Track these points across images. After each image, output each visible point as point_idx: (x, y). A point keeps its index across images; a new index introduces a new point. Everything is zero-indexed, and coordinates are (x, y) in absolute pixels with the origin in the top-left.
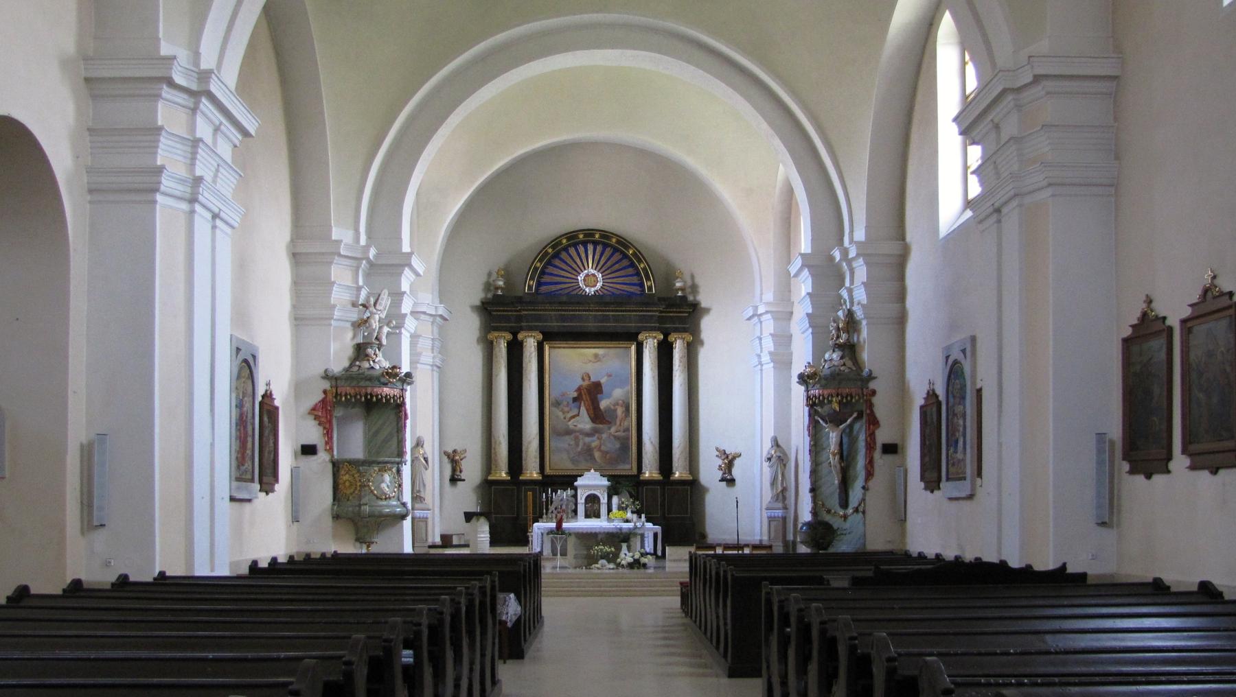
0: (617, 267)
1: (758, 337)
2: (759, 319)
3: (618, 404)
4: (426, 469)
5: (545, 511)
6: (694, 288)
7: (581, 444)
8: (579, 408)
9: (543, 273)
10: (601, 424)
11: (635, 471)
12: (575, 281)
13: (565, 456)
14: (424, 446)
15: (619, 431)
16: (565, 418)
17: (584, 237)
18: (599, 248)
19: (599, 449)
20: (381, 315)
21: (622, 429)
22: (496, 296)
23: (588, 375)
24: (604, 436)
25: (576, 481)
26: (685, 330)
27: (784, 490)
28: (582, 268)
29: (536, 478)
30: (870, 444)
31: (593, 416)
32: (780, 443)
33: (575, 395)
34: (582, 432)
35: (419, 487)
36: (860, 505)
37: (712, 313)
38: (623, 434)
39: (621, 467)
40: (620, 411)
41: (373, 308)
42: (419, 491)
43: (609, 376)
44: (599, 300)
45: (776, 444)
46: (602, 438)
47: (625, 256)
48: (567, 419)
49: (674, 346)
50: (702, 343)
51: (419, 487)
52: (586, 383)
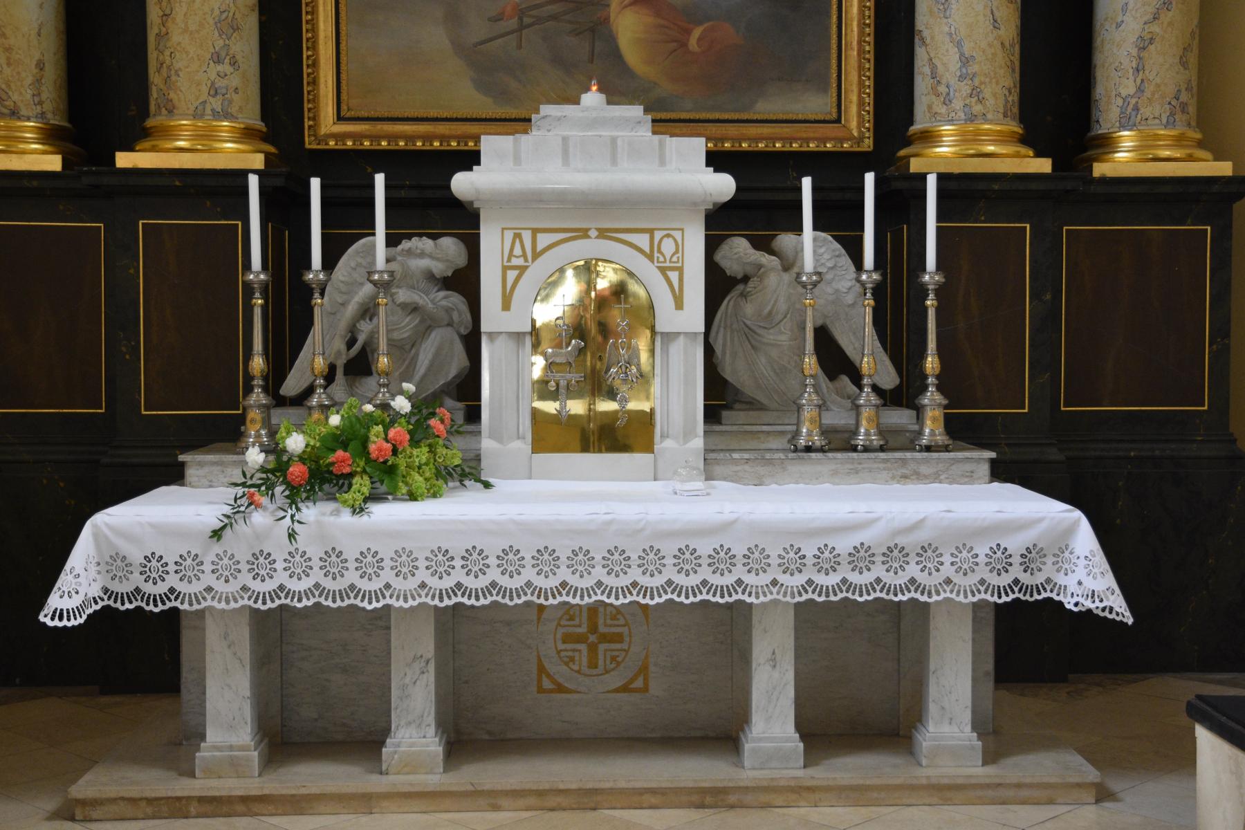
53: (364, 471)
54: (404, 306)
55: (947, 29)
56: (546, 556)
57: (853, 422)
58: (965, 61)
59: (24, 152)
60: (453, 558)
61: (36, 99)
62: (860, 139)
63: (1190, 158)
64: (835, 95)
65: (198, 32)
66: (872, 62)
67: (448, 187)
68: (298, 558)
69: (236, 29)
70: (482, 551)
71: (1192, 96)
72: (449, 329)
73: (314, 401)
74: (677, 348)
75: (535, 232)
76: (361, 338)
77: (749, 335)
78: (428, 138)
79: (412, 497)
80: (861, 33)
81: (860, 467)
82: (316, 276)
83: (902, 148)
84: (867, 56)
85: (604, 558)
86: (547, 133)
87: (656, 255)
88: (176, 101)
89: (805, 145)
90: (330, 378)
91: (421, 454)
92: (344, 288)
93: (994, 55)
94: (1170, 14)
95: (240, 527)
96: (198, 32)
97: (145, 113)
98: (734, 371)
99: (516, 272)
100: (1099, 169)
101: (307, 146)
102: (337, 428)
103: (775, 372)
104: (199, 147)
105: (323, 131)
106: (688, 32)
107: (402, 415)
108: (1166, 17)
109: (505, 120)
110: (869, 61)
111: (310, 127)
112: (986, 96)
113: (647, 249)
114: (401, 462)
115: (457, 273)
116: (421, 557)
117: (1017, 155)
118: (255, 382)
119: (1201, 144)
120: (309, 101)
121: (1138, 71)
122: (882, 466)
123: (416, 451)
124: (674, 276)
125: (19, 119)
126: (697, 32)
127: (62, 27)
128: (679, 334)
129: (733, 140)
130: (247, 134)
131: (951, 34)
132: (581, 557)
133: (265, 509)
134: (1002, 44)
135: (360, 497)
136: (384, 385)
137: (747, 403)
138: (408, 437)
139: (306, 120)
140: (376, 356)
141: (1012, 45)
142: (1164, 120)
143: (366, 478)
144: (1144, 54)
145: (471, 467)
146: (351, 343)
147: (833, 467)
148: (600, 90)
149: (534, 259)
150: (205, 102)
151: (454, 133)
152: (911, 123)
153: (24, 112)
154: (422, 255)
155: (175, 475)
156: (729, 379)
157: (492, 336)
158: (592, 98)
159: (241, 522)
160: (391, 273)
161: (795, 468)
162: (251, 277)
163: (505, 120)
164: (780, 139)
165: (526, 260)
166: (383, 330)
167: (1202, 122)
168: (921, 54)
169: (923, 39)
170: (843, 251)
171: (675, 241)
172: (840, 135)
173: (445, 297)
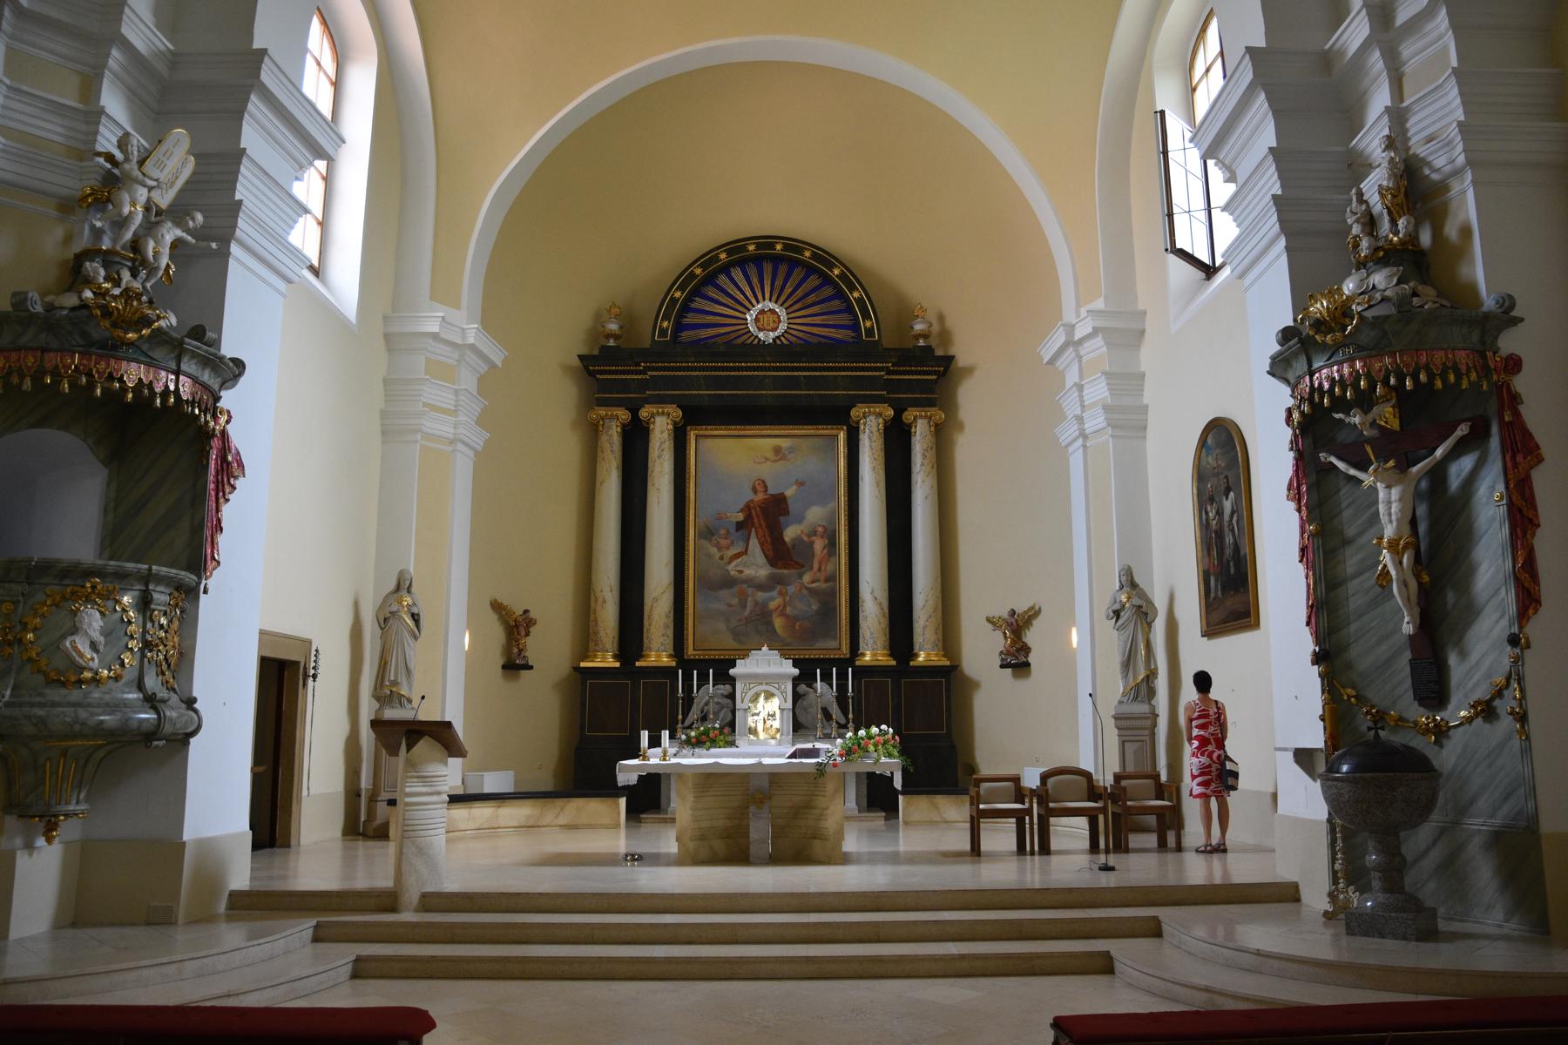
0: (812, 298)
1: (1075, 384)
2: (1077, 351)
3: (815, 533)
4: (416, 638)
5: (680, 717)
6: (946, 336)
7: (750, 603)
8: (748, 540)
9: (686, 308)
10: (785, 568)
13: (722, 626)
14: (413, 589)
15: (818, 581)
16: (722, 558)
17: (758, 248)
18: (783, 269)
19: (783, 614)
20: (156, 195)
21: (822, 576)
22: (604, 349)
23: (764, 482)
24: (791, 589)
25: (734, 666)
26: (930, 403)
27: (1151, 675)
28: (754, 301)
29: (669, 665)
30: (1520, 510)
31: (771, 553)
32: (1137, 580)
33: (741, 517)
34: (750, 582)
35: (396, 674)
36: (1499, 693)
37: (977, 373)
38: (825, 586)
40: (819, 545)
41: (136, 167)
42: (395, 683)
43: (800, 484)
44: (781, 351)
45: (1130, 582)
46: (787, 593)
47: (827, 280)
48: (726, 559)
49: (913, 430)
50: (960, 427)
51: (396, 674)
52: (761, 496)
58: (872, 634)
74: (785, 712)
78: (720, 655)
79: (720, 747)
91: (722, 737)
97: (642, 651)
98: (801, 719)
100: (912, 663)
105: (689, 653)
115: (730, 694)
119: (944, 656)
126: (798, 624)
130: (670, 656)
154: (721, 689)
157: (739, 710)
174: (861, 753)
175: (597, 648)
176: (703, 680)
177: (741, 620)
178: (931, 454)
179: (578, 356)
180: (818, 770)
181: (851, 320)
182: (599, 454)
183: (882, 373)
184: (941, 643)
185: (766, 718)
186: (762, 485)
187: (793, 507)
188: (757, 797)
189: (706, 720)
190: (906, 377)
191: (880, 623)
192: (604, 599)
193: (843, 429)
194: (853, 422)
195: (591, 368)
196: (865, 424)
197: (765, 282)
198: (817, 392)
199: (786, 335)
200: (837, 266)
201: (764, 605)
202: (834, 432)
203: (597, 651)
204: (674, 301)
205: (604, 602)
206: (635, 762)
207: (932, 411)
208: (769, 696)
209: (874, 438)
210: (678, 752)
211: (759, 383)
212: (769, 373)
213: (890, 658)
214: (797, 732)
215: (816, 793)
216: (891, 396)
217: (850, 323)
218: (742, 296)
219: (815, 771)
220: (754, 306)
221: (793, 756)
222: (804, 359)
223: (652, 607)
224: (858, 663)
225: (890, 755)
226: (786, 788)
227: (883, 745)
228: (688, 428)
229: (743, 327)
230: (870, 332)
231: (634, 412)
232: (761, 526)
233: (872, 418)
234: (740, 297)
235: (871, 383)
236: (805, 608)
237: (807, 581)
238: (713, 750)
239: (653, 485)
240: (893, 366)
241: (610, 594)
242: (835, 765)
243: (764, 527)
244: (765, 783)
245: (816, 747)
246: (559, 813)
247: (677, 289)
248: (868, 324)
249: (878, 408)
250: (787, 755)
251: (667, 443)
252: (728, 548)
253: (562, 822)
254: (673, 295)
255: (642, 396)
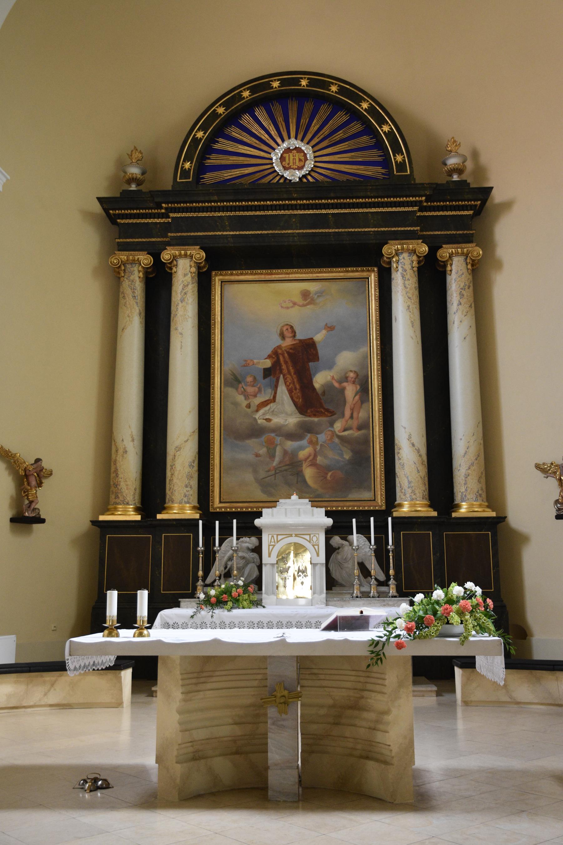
3: (345, 379)
5: (200, 573)
6: (480, 171)
8: (276, 387)
9: (208, 150)
10: (315, 416)
11: (380, 503)
12: (268, 161)
13: (249, 477)
16: (249, 406)
19: (313, 464)
21: (355, 423)
23: (292, 327)
24: (322, 438)
26: (468, 239)
28: (279, 141)
33: (268, 363)
34: (278, 430)
37: (516, 208)
39: (354, 496)
40: (350, 391)
43: (330, 328)
46: (317, 441)
47: (355, 115)
48: (253, 408)
49: (449, 268)
50: (499, 265)
52: (289, 342)
53: (231, 601)
54: (241, 557)
55: (403, 473)
56: (280, 623)
57: (370, 590)
58: (410, 482)
59: (130, 515)
60: (254, 624)
61: (134, 499)
62: (382, 506)
63: (484, 511)
64: (373, 492)
65: (181, 479)
66: (384, 482)
67: (254, 523)
68: (213, 623)
69: (192, 477)
70: (262, 622)
71: (483, 492)
72: (253, 564)
73: (216, 584)
74: (318, 568)
75: (277, 535)
76: (228, 567)
77: (340, 565)
78: (247, 508)
79: (243, 608)
80: (381, 473)
81: (371, 602)
82: (217, 548)
83: (393, 509)
84: (383, 480)
85: (295, 624)
86: (281, 507)
87: (311, 541)
88: (174, 499)
89: (358, 508)
90: (220, 577)
91: (246, 596)
92: (224, 553)
93: (418, 481)
94: (474, 467)
95: (198, 615)
96: (181, 479)
97: (165, 503)
98: (335, 575)
99: (272, 547)
100: (454, 515)
101: (211, 511)
102: (224, 588)
103: (348, 575)
104: (180, 512)
105: (215, 506)
106: (327, 474)
107: (240, 586)
108: (472, 468)
109: (271, 502)
110: (383, 482)
111: (211, 505)
112: (417, 493)
113: (309, 539)
114: (241, 598)
115: (256, 547)
116: (246, 624)
117: (428, 511)
118: (200, 578)
119: (488, 507)
120: (211, 497)
121: (465, 484)
122: (378, 602)
123: (244, 596)
124: (316, 547)
125: (129, 505)
126: (330, 474)
127: (141, 478)
128: (318, 564)
129: (341, 507)
130: (194, 508)
131: (405, 475)
132: (289, 623)
133: (205, 610)
134: (421, 477)
135: (230, 607)
136: (235, 579)
137: (340, 585)
138: (242, 591)
139: (210, 503)
140: (233, 572)
141: (424, 477)
142: (474, 499)
143: (231, 602)
144: (467, 479)
145: (259, 602)
146: (226, 568)
147: (364, 602)
148: (296, 495)
149: (277, 543)
150: (182, 499)
151: (255, 506)
152: (396, 501)
153: (130, 503)
154: (246, 542)
155: (178, 605)
156: (334, 577)
157: (266, 564)
158: (294, 497)
159: (199, 613)
160: (238, 547)
161: (352, 603)
162: (199, 549)
163: (271, 502)
164: (356, 506)
165: (275, 543)
166: (235, 563)
167: (488, 500)
168: (397, 479)
169: (397, 476)
170: (367, 540)
171: (317, 537)
172: (375, 505)
173: (253, 555)
174: (441, 627)
175: (118, 501)
176: (226, 532)
177: (268, 471)
178: (469, 293)
179: (99, 199)
180: (372, 652)
181: (381, 156)
182: (122, 301)
183: (416, 208)
184: (485, 492)
185: (296, 574)
186: (290, 330)
187: (322, 352)
188: (279, 695)
189: (230, 577)
190: (441, 213)
191: (418, 471)
192: (125, 448)
193: (374, 271)
194: (384, 262)
195: (111, 212)
196: (397, 262)
197: (290, 120)
198: (346, 230)
199: (313, 174)
200: (365, 100)
201: (294, 454)
202: (365, 274)
203: (118, 504)
204: (196, 141)
205: (126, 452)
206: (97, 638)
207: (467, 247)
208: (299, 549)
209: (408, 277)
210: (195, 613)
211: (286, 222)
212: (296, 212)
213: (430, 509)
214: (331, 589)
215: (369, 687)
216: (425, 233)
217: (380, 159)
218: (266, 136)
219: (368, 654)
220: (278, 145)
221: (333, 626)
222: (332, 195)
223: (175, 456)
224: (395, 514)
225: (482, 629)
226: (322, 677)
227: (471, 612)
228: (213, 273)
229: (269, 166)
230: (401, 166)
231: (156, 256)
232: (289, 372)
233: (405, 255)
234: (265, 137)
235: (402, 219)
236: (337, 457)
237: (339, 428)
238: (236, 612)
239: (176, 329)
240: (426, 201)
241: (131, 444)
242: (400, 646)
243: (292, 374)
244: (291, 672)
245: (365, 613)
246: (49, 690)
247: (199, 129)
248: (399, 158)
249: (412, 244)
250: (325, 624)
251: (190, 287)
252: (255, 396)
253: (51, 702)
254: (195, 135)
255: (164, 239)
